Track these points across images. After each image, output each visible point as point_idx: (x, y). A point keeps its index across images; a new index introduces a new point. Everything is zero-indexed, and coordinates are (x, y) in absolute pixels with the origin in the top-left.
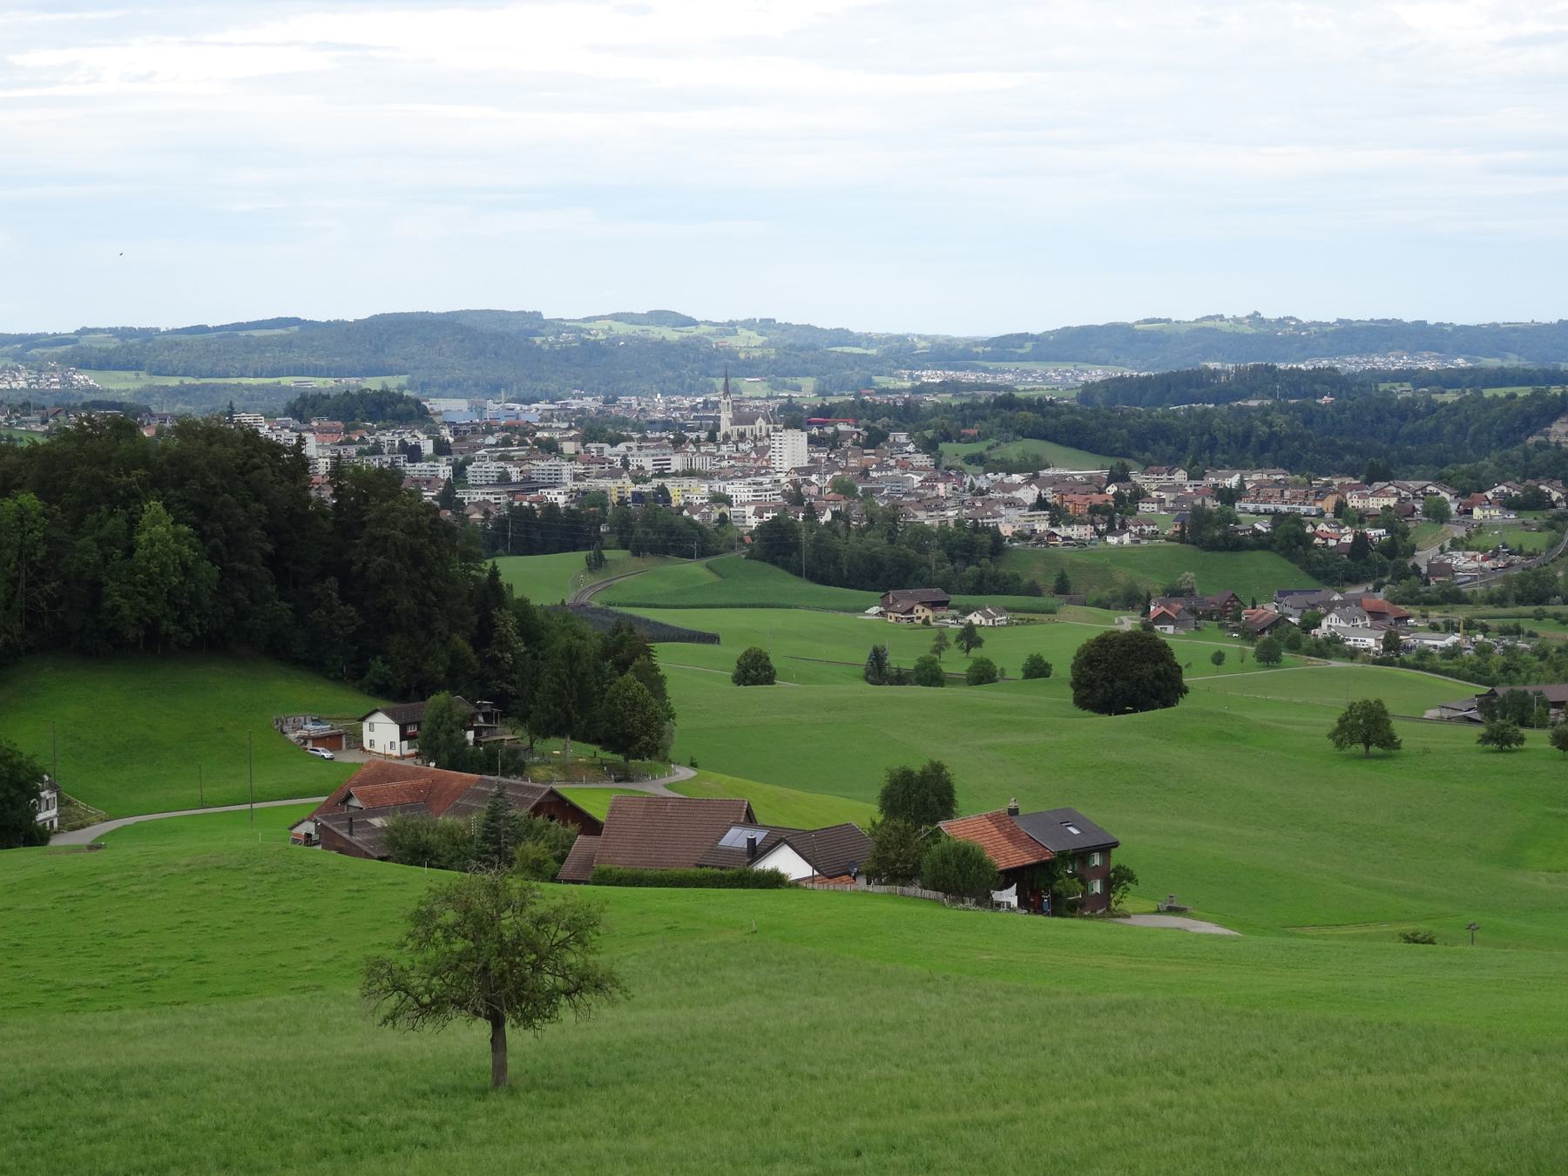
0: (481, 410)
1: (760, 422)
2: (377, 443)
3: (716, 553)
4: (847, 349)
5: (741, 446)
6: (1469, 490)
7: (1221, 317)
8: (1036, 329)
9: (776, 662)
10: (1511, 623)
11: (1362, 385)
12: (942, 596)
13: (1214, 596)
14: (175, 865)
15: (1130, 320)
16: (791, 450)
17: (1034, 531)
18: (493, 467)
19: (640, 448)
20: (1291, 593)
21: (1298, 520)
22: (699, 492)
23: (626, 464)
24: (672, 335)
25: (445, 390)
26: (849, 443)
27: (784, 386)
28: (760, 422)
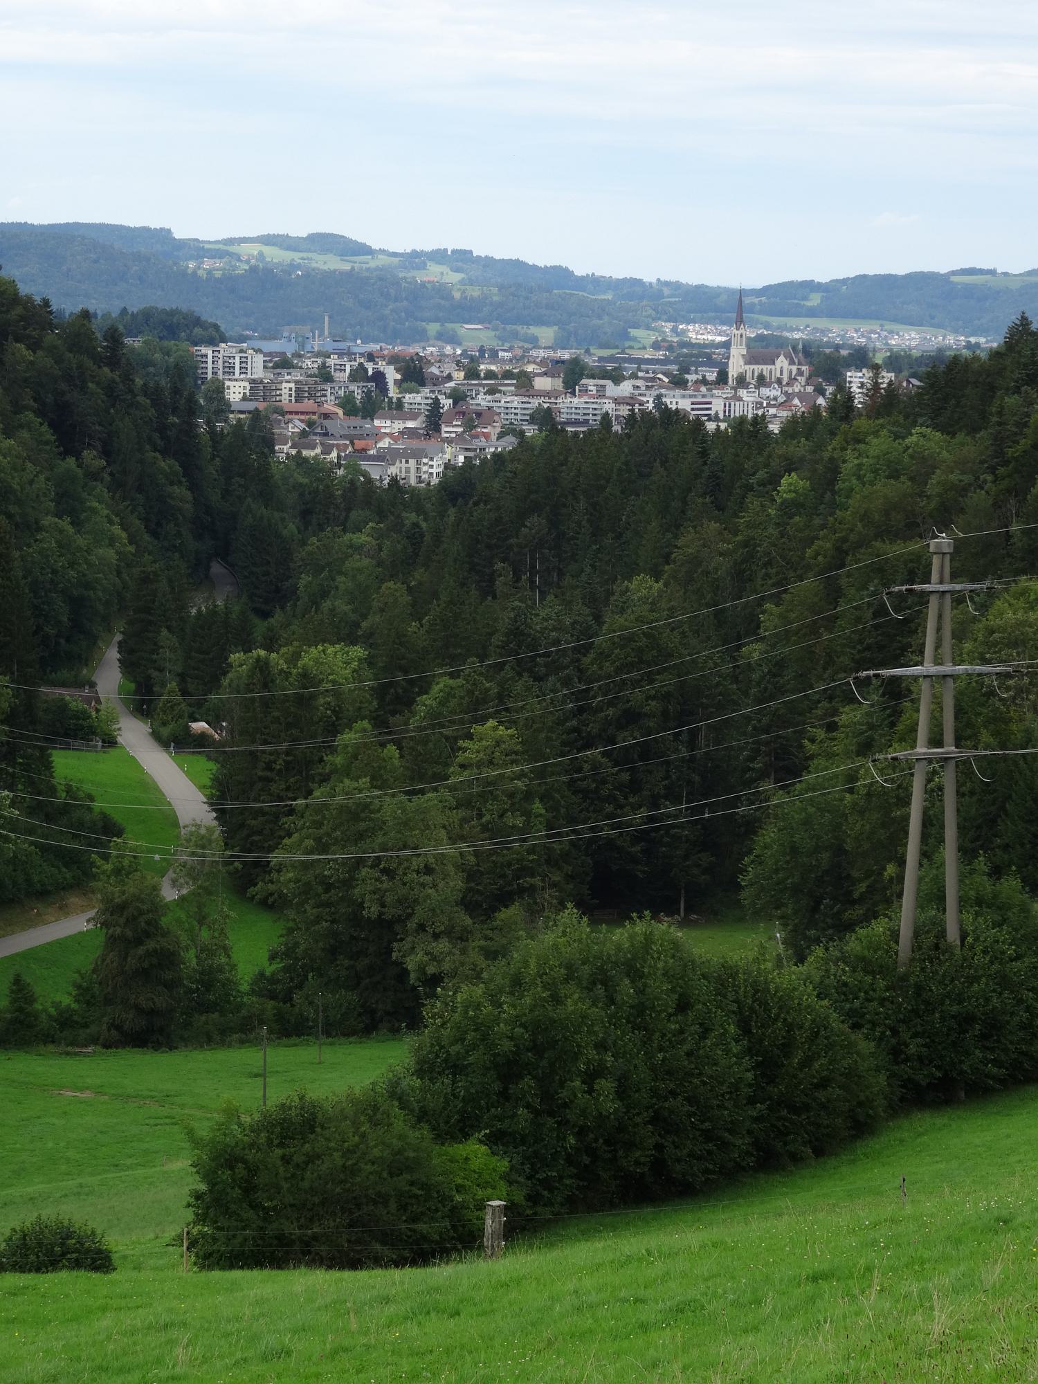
1: (782, 362)
14: (156, 1269)
28: (782, 362)
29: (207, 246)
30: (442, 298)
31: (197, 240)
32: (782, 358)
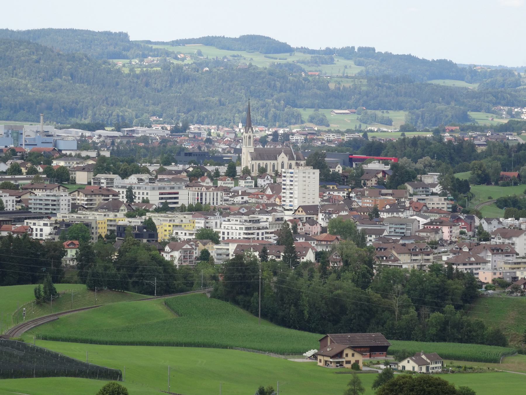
4: (449, 83)
5: (260, 182)
16: (302, 187)
17: (515, 279)
19: (151, 181)
22: (187, 228)
24: (261, 61)
26: (373, 182)
27: (374, 120)
29: (154, 47)
30: (319, 88)
31: (149, 42)
32: (283, 155)
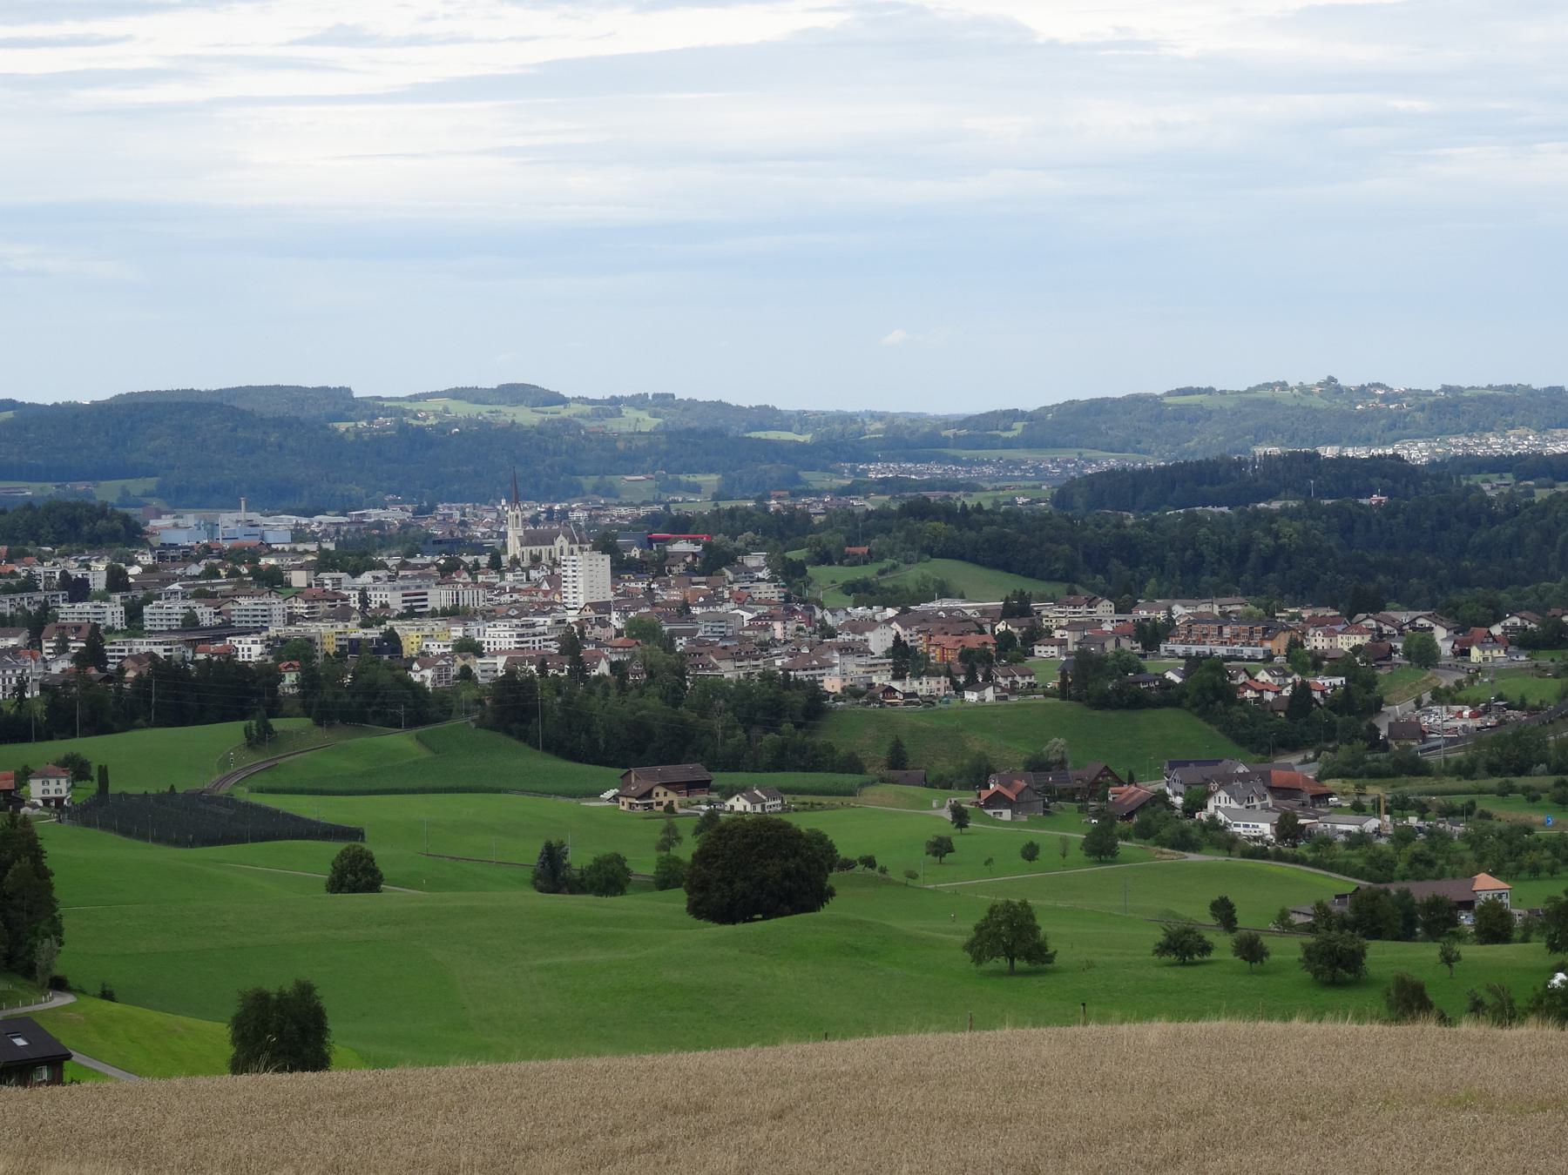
0: (212, 528)
2: (30, 576)
3: (437, 721)
4: (772, 435)
5: (533, 574)
6: (1466, 626)
7: (1283, 385)
8: (1029, 404)
9: (384, 868)
10: (1459, 801)
11: (1438, 478)
12: (703, 775)
13: (1083, 768)
15: (1159, 390)
16: (585, 580)
18: (178, 608)
20: (1186, 764)
21: (1216, 665)
23: (364, 600)
24: (526, 417)
25: (179, 498)
27: (678, 487)
29: (387, 404)
31: (379, 398)
32: (561, 537)
